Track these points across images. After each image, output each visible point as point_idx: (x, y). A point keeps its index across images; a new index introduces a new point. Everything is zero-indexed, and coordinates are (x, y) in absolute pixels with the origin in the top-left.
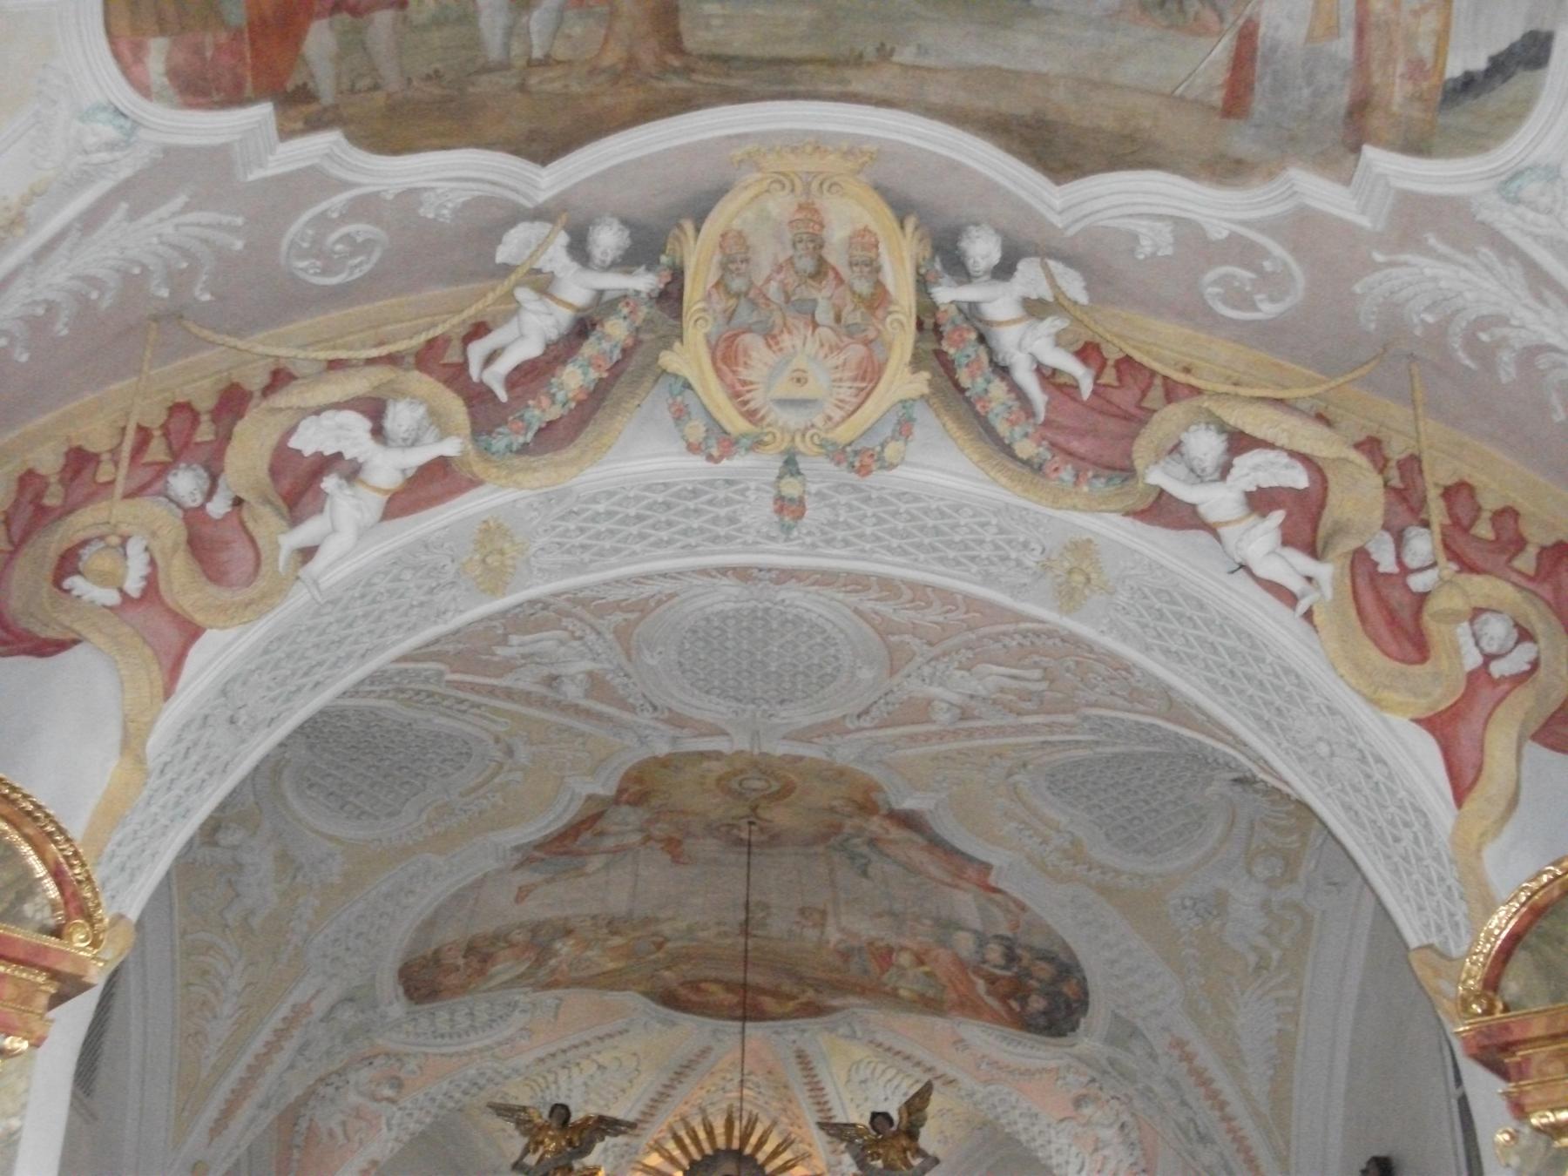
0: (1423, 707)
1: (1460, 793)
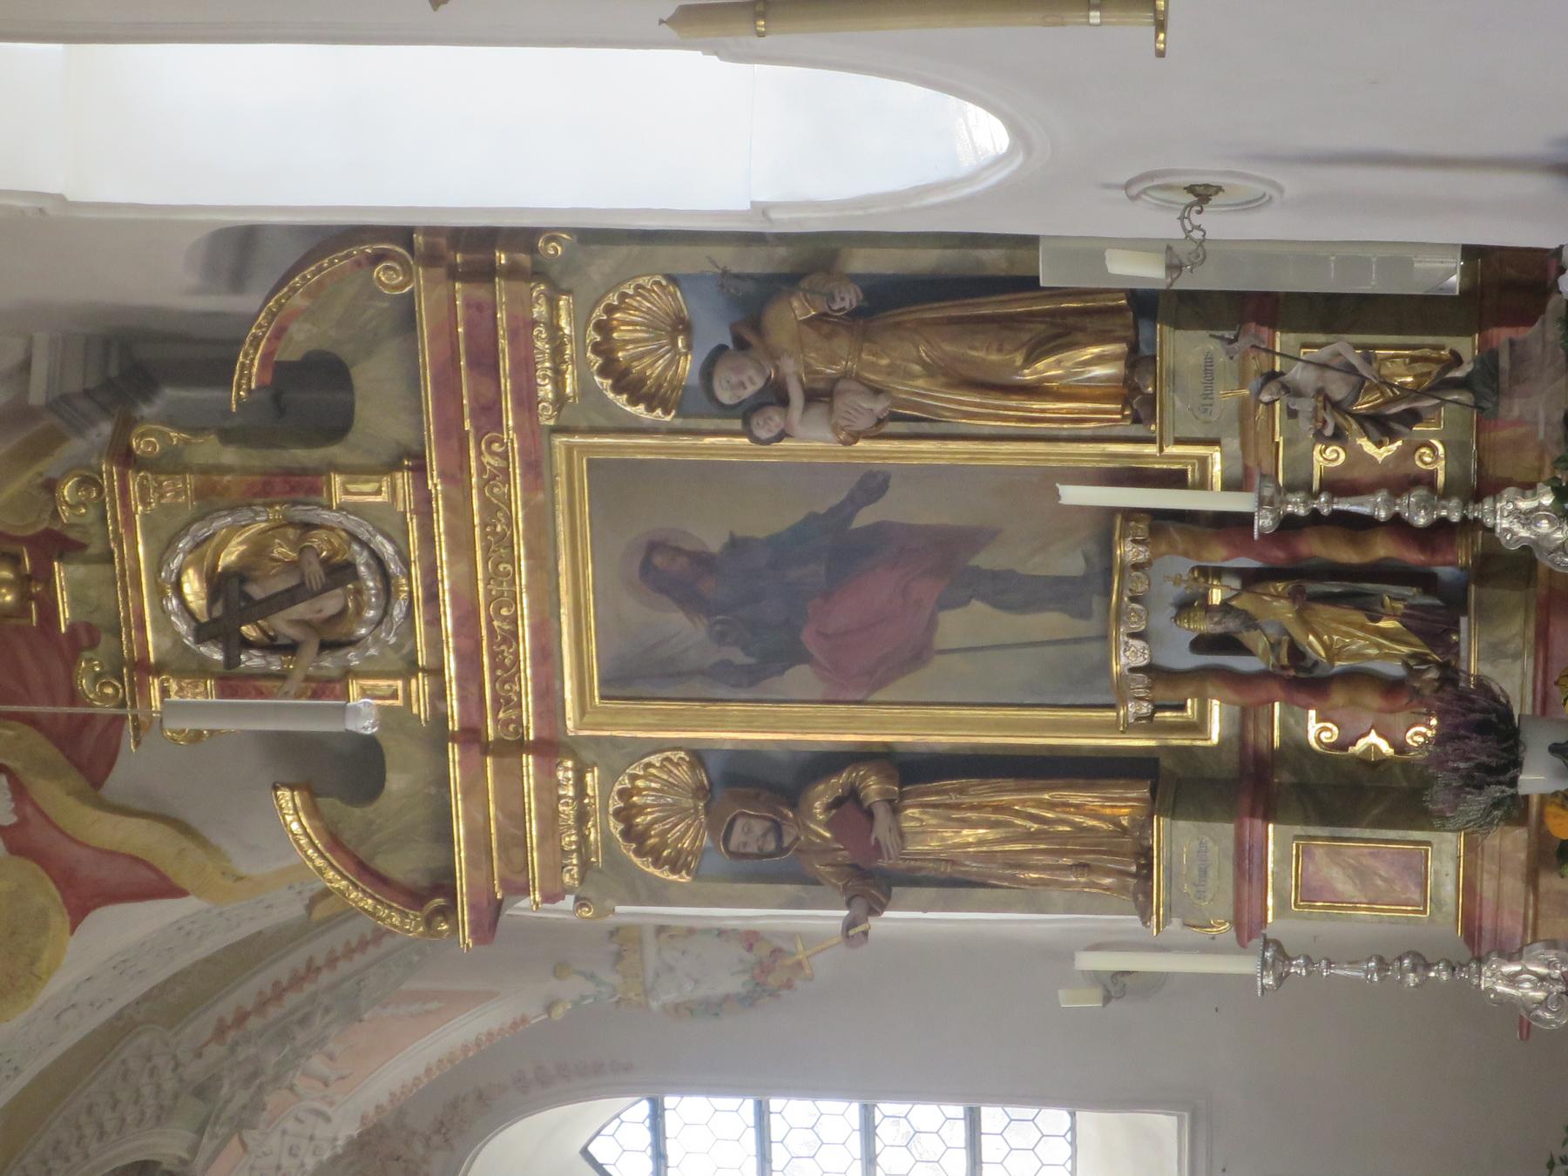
0: (60, 920)
1: (176, 892)
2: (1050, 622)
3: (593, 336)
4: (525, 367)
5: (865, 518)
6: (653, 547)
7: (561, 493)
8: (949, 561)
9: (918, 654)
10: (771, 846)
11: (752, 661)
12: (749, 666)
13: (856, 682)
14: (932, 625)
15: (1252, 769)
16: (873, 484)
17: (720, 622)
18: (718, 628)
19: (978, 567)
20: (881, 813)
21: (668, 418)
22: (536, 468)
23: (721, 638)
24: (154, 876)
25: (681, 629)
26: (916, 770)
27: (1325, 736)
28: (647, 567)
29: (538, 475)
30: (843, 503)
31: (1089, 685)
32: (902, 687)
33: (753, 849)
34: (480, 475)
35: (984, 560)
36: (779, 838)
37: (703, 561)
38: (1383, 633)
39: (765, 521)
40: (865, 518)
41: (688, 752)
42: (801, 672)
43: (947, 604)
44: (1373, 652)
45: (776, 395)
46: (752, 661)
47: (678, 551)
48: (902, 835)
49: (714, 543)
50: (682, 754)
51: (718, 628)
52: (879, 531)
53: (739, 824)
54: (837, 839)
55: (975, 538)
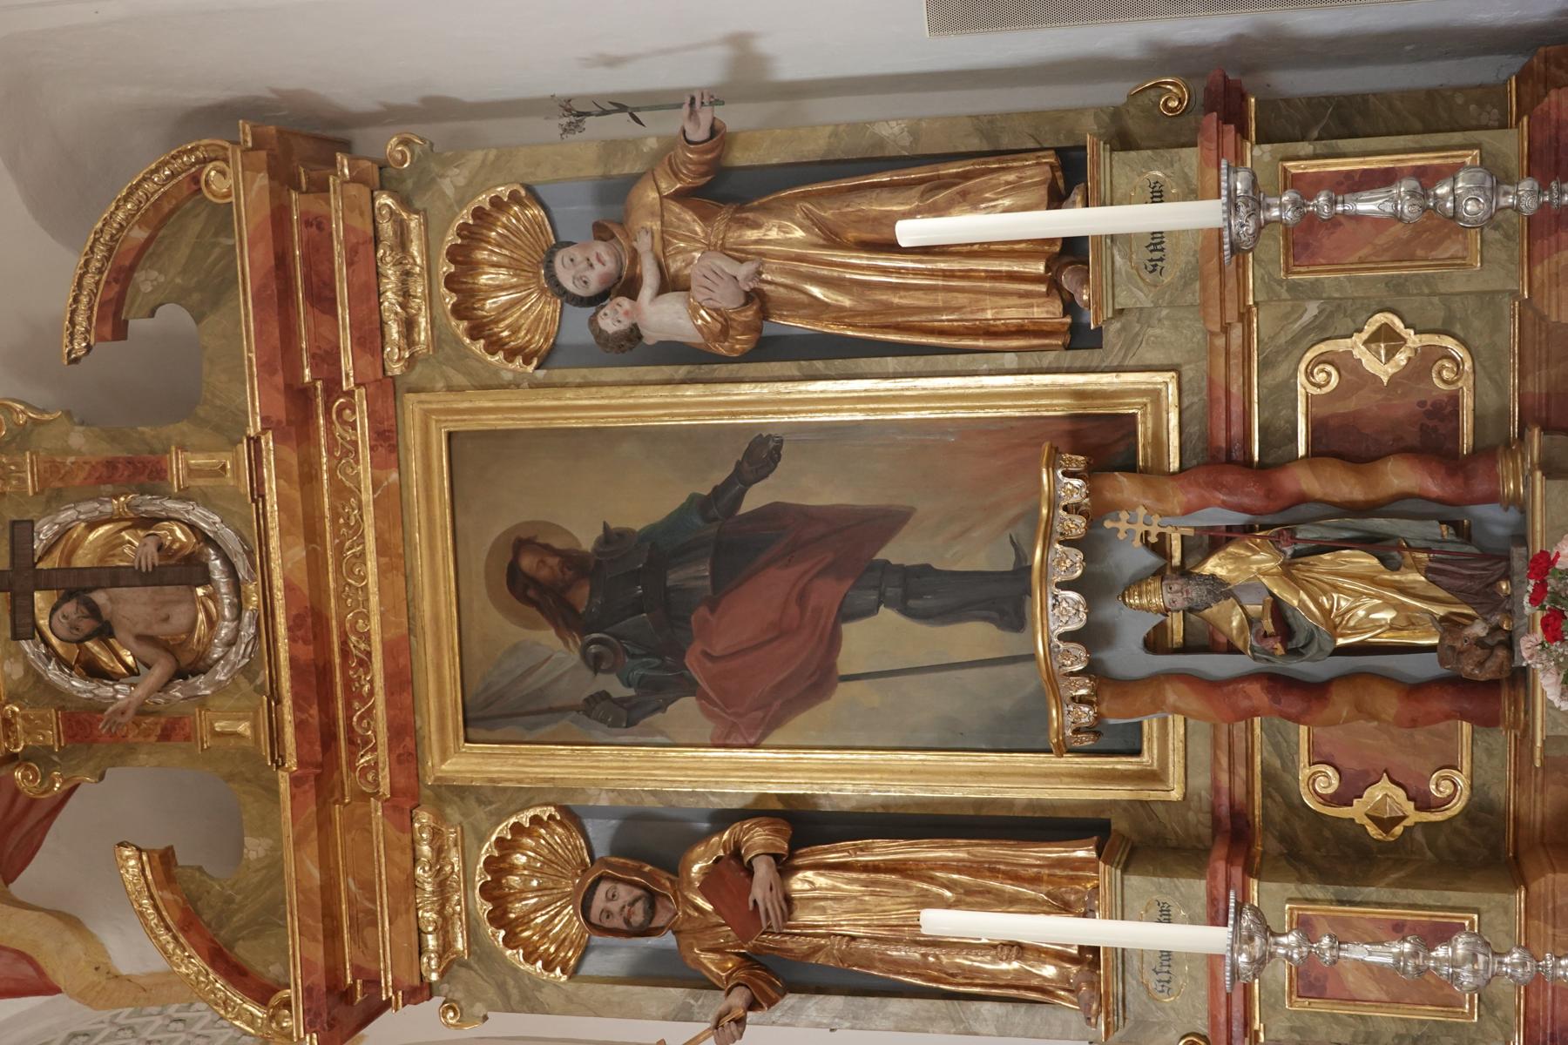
1: (45, 987)
2: (975, 637)
3: (447, 268)
4: (367, 294)
5: (755, 498)
6: (522, 543)
7: (415, 466)
8: (850, 558)
9: (820, 679)
10: (638, 918)
11: (631, 692)
12: (629, 699)
13: (747, 722)
14: (833, 642)
15: (1227, 823)
16: (762, 452)
17: (594, 641)
18: (593, 649)
19: (887, 562)
20: (763, 870)
21: (530, 369)
22: (387, 439)
23: (594, 664)
24: (30, 971)
25: (552, 650)
26: (805, 827)
27: (1321, 786)
28: (513, 571)
29: (394, 448)
30: (729, 482)
31: (1019, 731)
32: (802, 721)
33: (617, 922)
34: (330, 452)
35: (899, 551)
36: (651, 910)
37: (573, 560)
38: (1402, 589)
39: (646, 503)
40: (755, 498)
41: (560, 808)
42: (687, 705)
43: (849, 613)
44: (1387, 615)
45: (627, 286)
46: (631, 692)
47: (548, 549)
48: (788, 900)
49: (587, 540)
50: (552, 810)
51: (593, 649)
52: (773, 513)
53: (604, 888)
54: (717, 910)
55: (888, 522)
